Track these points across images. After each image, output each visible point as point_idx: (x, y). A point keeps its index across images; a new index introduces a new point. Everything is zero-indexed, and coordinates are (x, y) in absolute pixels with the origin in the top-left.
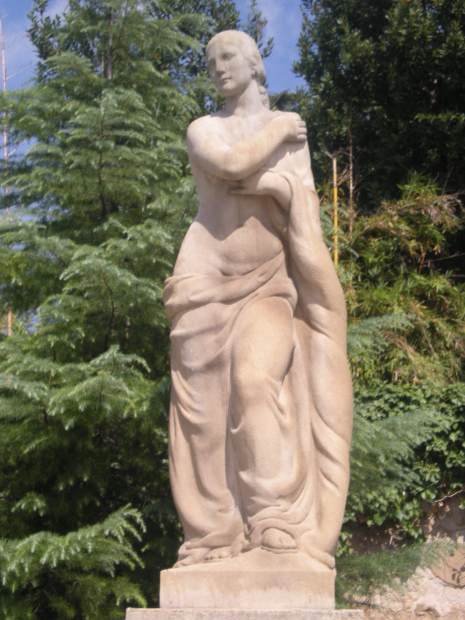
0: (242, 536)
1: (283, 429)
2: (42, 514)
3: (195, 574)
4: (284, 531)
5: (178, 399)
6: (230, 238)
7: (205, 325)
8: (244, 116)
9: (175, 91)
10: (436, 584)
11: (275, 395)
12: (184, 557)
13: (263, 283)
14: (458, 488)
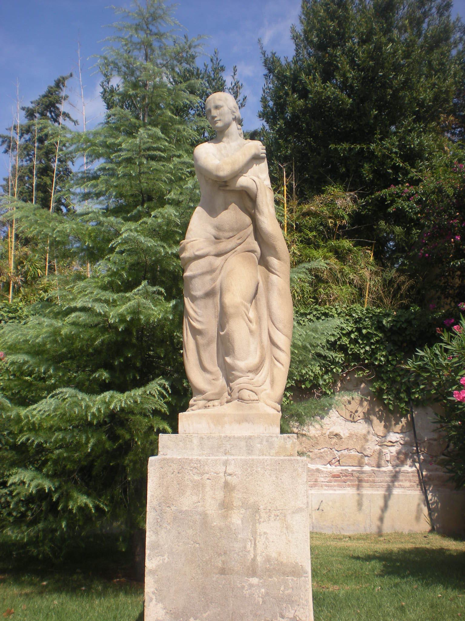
0: (226, 394)
1: (251, 332)
2: (107, 381)
3: (199, 415)
4: (251, 391)
5: (188, 314)
6: (219, 216)
7: (205, 270)
8: (229, 143)
9: (185, 127)
10: (341, 420)
11: (247, 312)
12: (193, 405)
13: (240, 244)
14: (355, 365)
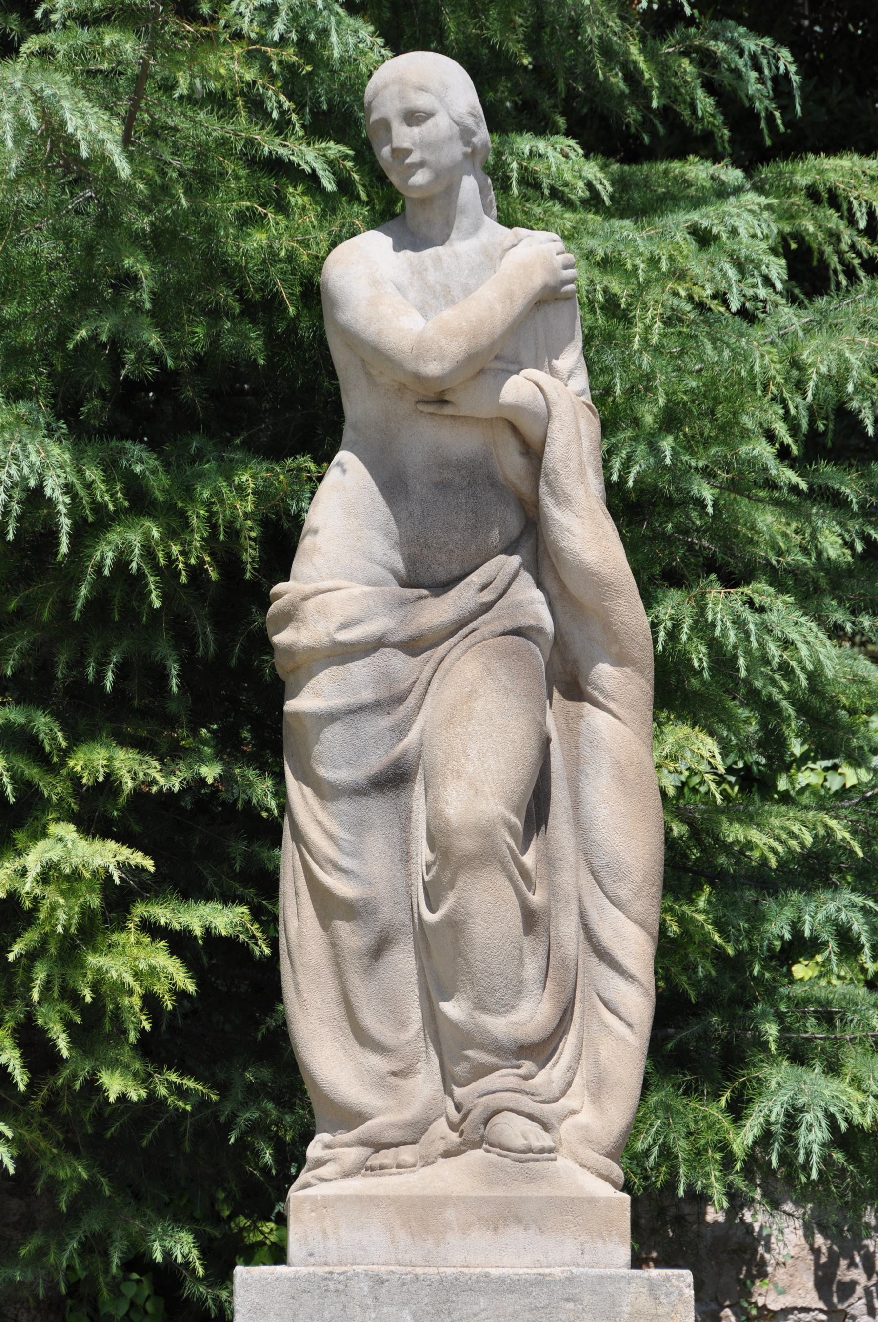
12: (320, 1163)
